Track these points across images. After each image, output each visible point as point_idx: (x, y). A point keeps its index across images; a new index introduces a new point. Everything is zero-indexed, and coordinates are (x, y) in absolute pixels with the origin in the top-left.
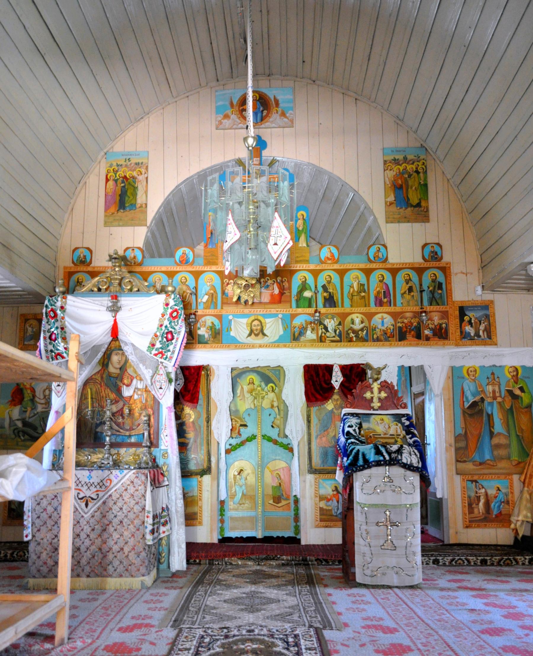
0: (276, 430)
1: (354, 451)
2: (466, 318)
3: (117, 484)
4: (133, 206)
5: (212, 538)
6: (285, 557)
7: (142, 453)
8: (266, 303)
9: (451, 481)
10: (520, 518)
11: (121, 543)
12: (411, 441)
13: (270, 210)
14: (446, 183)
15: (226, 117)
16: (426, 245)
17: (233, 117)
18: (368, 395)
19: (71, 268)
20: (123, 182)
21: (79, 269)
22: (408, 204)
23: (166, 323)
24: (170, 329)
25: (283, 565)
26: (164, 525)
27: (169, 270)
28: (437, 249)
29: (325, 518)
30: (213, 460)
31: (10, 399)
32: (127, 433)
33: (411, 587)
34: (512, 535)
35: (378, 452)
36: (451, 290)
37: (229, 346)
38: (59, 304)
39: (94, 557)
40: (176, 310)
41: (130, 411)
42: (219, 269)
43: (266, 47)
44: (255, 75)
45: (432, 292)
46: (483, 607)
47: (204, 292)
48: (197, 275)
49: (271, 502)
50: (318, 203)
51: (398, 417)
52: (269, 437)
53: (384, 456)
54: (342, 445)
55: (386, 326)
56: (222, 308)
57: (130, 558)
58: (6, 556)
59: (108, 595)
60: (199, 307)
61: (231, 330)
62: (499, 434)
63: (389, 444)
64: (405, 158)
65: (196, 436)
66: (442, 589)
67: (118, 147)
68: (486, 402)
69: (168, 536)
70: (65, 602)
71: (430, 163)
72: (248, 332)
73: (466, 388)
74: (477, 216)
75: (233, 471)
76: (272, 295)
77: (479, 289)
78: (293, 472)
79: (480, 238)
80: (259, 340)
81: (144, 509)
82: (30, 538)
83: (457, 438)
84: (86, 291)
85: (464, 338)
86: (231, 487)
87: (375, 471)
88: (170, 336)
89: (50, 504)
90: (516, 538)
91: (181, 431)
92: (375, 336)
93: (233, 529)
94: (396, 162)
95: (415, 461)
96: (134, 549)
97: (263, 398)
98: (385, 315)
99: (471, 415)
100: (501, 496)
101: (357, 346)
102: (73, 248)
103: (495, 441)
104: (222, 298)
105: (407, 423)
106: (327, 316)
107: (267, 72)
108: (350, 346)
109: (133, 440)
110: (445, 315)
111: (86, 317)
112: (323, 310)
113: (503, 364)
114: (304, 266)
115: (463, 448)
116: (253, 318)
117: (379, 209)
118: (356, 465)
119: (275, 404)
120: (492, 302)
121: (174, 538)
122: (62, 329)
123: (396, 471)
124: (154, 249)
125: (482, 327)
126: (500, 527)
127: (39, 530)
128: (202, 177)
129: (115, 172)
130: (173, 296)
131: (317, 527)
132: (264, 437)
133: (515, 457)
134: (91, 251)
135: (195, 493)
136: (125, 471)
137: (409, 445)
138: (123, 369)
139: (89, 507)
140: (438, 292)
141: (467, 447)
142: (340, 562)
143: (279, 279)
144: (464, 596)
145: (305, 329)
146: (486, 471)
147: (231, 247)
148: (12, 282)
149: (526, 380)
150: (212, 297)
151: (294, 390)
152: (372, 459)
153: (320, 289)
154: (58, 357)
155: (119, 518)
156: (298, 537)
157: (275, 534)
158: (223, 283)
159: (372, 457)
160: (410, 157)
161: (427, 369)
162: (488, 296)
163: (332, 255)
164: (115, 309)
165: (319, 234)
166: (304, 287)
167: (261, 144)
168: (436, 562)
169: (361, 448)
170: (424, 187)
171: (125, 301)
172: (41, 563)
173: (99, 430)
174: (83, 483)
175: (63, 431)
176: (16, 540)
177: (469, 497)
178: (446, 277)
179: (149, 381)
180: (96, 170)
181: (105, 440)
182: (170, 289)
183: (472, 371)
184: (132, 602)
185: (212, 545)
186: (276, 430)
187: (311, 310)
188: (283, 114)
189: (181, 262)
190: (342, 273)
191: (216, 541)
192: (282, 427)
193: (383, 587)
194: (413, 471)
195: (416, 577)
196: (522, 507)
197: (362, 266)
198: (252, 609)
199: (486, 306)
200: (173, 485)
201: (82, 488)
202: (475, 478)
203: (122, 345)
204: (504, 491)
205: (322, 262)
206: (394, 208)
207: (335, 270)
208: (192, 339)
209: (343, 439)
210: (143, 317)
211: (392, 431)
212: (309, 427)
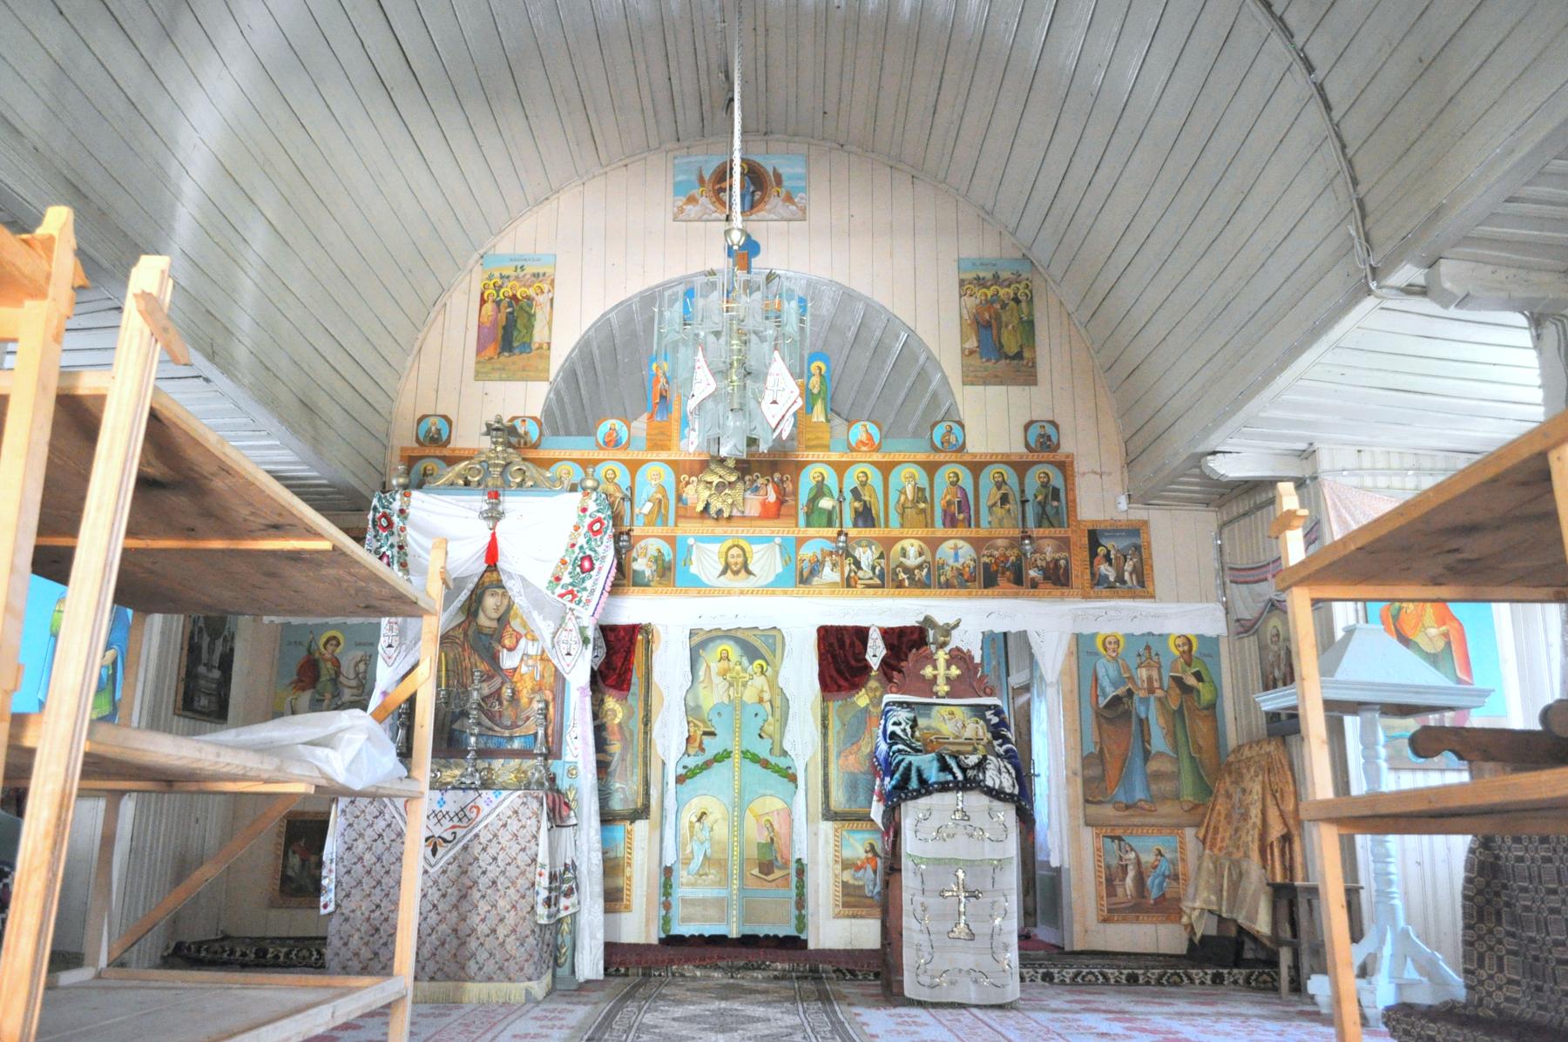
0: (767, 743)
1: (903, 764)
4: (526, 347)
6: (779, 966)
7: (531, 767)
8: (752, 518)
9: (1075, 837)
11: (492, 920)
12: (1001, 750)
13: (766, 347)
14: (1065, 321)
15: (692, 200)
16: (1031, 423)
17: (703, 200)
18: (928, 671)
20: (510, 305)
21: (427, 452)
22: (1000, 352)
23: (582, 541)
25: (776, 978)
26: (568, 894)
28: (1050, 430)
29: (852, 901)
31: (295, 677)
32: (507, 733)
33: (1000, 1007)
34: (1185, 936)
35: (945, 767)
38: (396, 505)
39: (443, 944)
40: (599, 520)
41: (514, 691)
43: (762, 88)
44: (744, 132)
45: (1043, 505)
47: (645, 496)
48: (634, 466)
49: (756, 871)
50: (846, 352)
51: (979, 711)
52: (754, 755)
53: (954, 774)
54: (882, 758)
55: (961, 561)
57: (508, 947)
58: (277, 957)
59: (468, 1009)
62: (1160, 754)
63: (963, 753)
64: (996, 277)
65: (625, 749)
66: (1055, 1011)
68: (1135, 698)
69: (574, 916)
71: (1037, 282)
72: (721, 568)
73: (1101, 672)
75: (689, 815)
76: (764, 504)
77: (1123, 501)
78: (796, 817)
79: (1124, 413)
80: (742, 582)
81: (534, 860)
82: (331, 908)
83: (1087, 761)
85: (1098, 584)
87: (937, 799)
88: (587, 564)
89: (370, 849)
91: (600, 730)
93: (685, 920)
94: (980, 282)
95: (1007, 783)
96: (514, 931)
97: (745, 685)
98: (961, 543)
99: (1110, 721)
100: (1164, 867)
101: (910, 596)
102: (418, 415)
104: (677, 508)
105: (995, 720)
106: (858, 542)
107: (763, 130)
109: (516, 745)
110: (1064, 544)
112: (853, 532)
113: (1166, 631)
115: (1097, 779)
116: (729, 543)
119: (767, 696)
120: (1145, 523)
122: (401, 547)
123: (976, 801)
124: (560, 423)
125: (1128, 566)
126: (1162, 922)
127: (348, 895)
128: (650, 298)
129: (498, 288)
131: (837, 916)
132: (745, 753)
133: (1188, 795)
134: (450, 422)
135: (621, 852)
136: (505, 793)
137: (998, 756)
138: (503, 621)
139: (439, 855)
140: (1053, 505)
141: (1102, 778)
142: (877, 975)
143: (777, 476)
145: (822, 564)
146: (1136, 820)
147: (700, 406)
149: (1207, 660)
151: (801, 670)
152: (932, 780)
153: (848, 495)
155: (490, 875)
157: (762, 931)
158: (678, 482)
159: (933, 775)
160: (1004, 275)
161: (1034, 640)
162: (1139, 514)
165: (848, 406)
166: (820, 490)
167: (746, 252)
168: (1048, 977)
169: (916, 760)
170: (1029, 326)
171: (510, 502)
173: (456, 726)
175: (412, 701)
176: (292, 934)
177: (1108, 867)
180: (465, 285)
181: (467, 744)
182: (590, 483)
183: (1111, 643)
184: (511, 1018)
185: (648, 947)
186: (767, 743)
188: (789, 199)
189: (606, 443)
190: (886, 468)
191: (654, 941)
192: (777, 737)
193: (952, 1005)
194: (1004, 800)
195: (1009, 989)
196: (1202, 883)
197: (921, 457)
199: (1135, 531)
200: (585, 825)
202: (1119, 832)
203: (504, 578)
204: (1168, 856)
205: (851, 449)
206: (976, 361)
207: (873, 463)
208: (623, 578)
209: (883, 747)
210: (540, 533)
211: (969, 733)
212: (825, 735)
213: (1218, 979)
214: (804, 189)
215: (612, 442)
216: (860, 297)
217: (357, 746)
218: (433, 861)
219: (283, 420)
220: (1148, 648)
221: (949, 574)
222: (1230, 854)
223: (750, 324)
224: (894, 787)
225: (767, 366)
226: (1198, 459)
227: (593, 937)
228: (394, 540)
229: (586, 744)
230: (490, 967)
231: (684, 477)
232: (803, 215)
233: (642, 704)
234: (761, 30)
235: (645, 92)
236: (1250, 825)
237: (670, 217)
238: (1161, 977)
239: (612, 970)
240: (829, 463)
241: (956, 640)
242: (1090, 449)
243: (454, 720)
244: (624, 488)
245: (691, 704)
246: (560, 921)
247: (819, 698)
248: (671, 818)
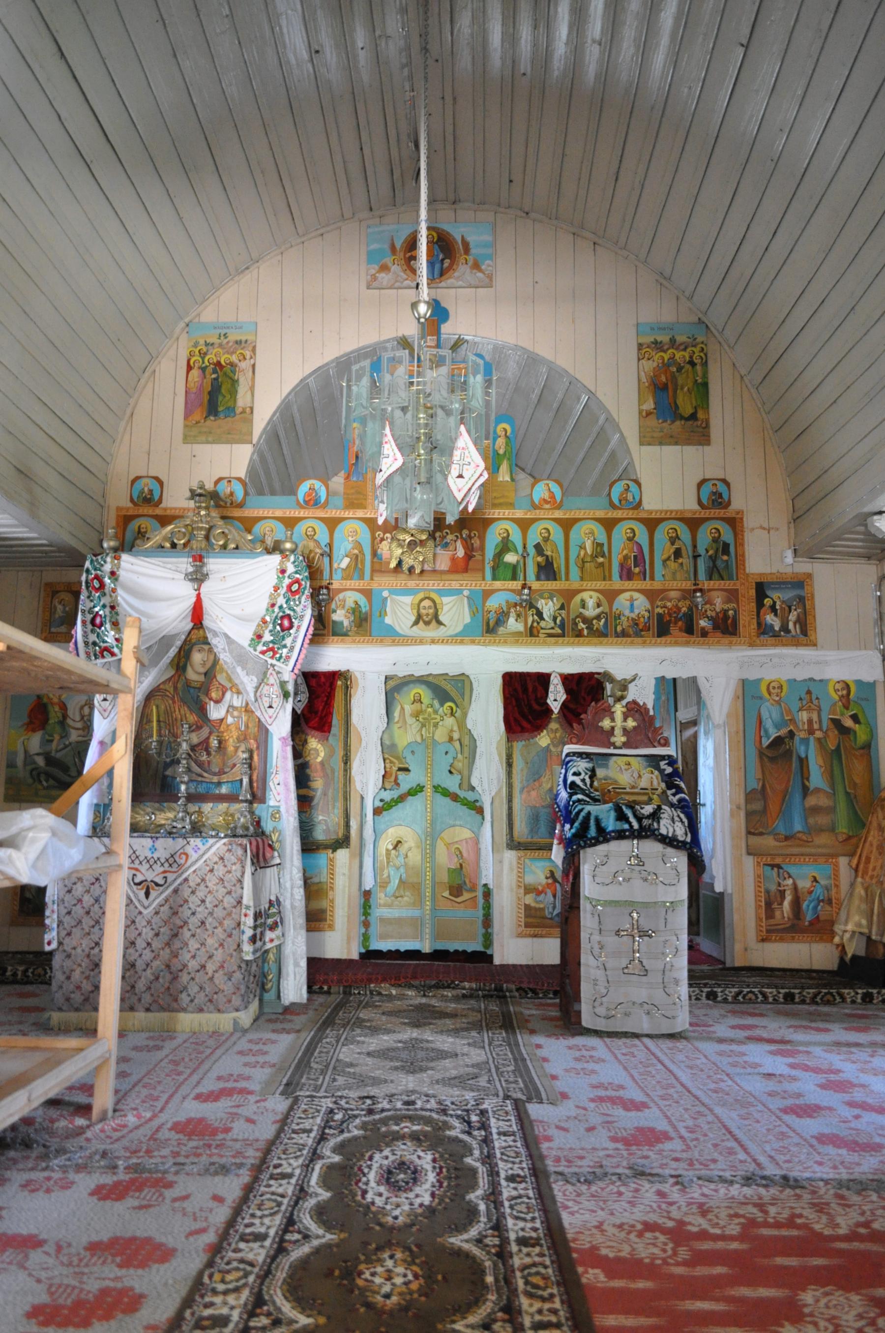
0: (457, 778)
1: (583, 814)
2: (767, 602)
3: (197, 861)
4: (231, 410)
5: (349, 951)
6: (467, 985)
8: (442, 572)
9: (738, 864)
11: (202, 957)
12: (675, 799)
13: (452, 421)
15: (384, 268)
17: (395, 268)
18: (606, 723)
19: (128, 509)
20: (215, 372)
22: (676, 415)
23: (281, 601)
24: (288, 612)
25: (464, 996)
26: (273, 928)
27: (287, 515)
28: (721, 488)
29: (533, 922)
31: (26, 720)
32: (215, 779)
33: (671, 1036)
34: (836, 954)
35: (621, 817)
36: (743, 555)
37: (381, 641)
38: (108, 568)
39: (157, 978)
40: (297, 581)
41: (220, 742)
42: (368, 516)
43: (450, 156)
44: (431, 201)
45: (713, 559)
46: (786, 1071)
47: (342, 552)
48: (332, 524)
49: (446, 894)
51: (653, 761)
53: (630, 824)
54: (562, 804)
55: (636, 611)
56: (372, 579)
57: (217, 981)
58: (15, 974)
59: (179, 1040)
60: (334, 576)
61: (386, 614)
62: (818, 790)
63: (638, 803)
64: (673, 341)
65: (327, 785)
66: (721, 1041)
67: (208, 315)
69: (279, 947)
70: (109, 1051)
71: (713, 349)
72: (413, 618)
73: (765, 715)
74: (788, 436)
75: (386, 844)
76: (453, 559)
78: (482, 846)
81: (239, 902)
82: (54, 945)
83: (750, 796)
84: (152, 547)
85: (764, 633)
86: (382, 870)
87: (615, 846)
88: (286, 623)
89: (88, 891)
92: (619, 629)
93: (383, 937)
94: (657, 346)
95: (681, 831)
96: (222, 967)
97: (436, 725)
98: (636, 595)
99: (772, 759)
100: (819, 892)
101: (588, 644)
102: (132, 477)
103: (811, 801)
104: (372, 563)
105: (669, 770)
106: (541, 594)
107: (451, 197)
108: (579, 644)
109: (224, 790)
110: (733, 595)
111: (151, 589)
112: (536, 585)
113: (826, 676)
114: (507, 513)
115: (758, 812)
116: (421, 595)
117: (629, 423)
119: (456, 736)
120: (810, 576)
121: (288, 950)
122: (113, 608)
123: (650, 848)
125: (793, 617)
126: (816, 942)
127: (69, 934)
129: (203, 355)
130: (292, 558)
131: (520, 935)
132: (436, 788)
133: (843, 828)
134: (161, 483)
135: (324, 877)
137: (672, 805)
138: (210, 674)
139: (151, 897)
140: (723, 559)
141: (765, 810)
142: (556, 993)
143: (465, 533)
144: (756, 1053)
145: (506, 615)
146: (796, 850)
149: (863, 703)
150: (357, 559)
151: (487, 714)
153: (532, 551)
154: (105, 653)
155: (199, 916)
156: (489, 952)
157: (452, 946)
158: (373, 538)
159: (611, 824)
161: (702, 684)
162: (804, 567)
163: (552, 496)
164: (198, 577)
166: (505, 546)
167: (439, 313)
168: (712, 996)
169: (594, 809)
170: (703, 389)
171: (215, 564)
173: (169, 772)
174: (141, 858)
175: (110, 773)
177: (767, 892)
178: (736, 535)
181: (179, 790)
182: (288, 545)
183: (774, 688)
184: (219, 1052)
186: (457, 778)
187: (517, 585)
188: (476, 266)
190: (567, 525)
191: (355, 956)
192: (466, 773)
194: (677, 847)
195: (679, 1020)
197: (600, 514)
198: (412, 1068)
199: (800, 583)
200: (288, 865)
201: (139, 867)
202: (778, 860)
203: (209, 636)
204: (823, 882)
205: (535, 507)
206: (653, 422)
208: (323, 629)
209: (564, 795)
210: (244, 591)
211: (644, 783)
212: (509, 774)
213: (868, 998)
214: (490, 257)
215: (312, 501)
217: (39, 846)
218: (146, 903)
220: (809, 692)
221: (625, 624)
223: (436, 399)
224: (574, 835)
227: (297, 965)
228: (105, 600)
229: (288, 790)
231: (379, 534)
235: (338, 158)
237: (363, 286)
238: (816, 995)
239: (316, 987)
240: (512, 520)
241: (632, 694)
242: (759, 506)
243: (167, 766)
246: (267, 952)
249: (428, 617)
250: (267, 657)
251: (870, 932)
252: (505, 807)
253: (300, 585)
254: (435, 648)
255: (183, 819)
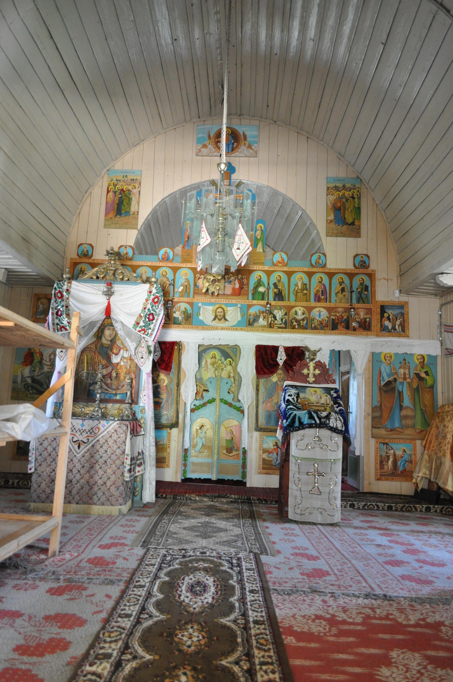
0: (232, 396)
1: (292, 415)
2: (386, 315)
4: (128, 213)
6: (233, 496)
9: (367, 442)
10: (420, 475)
11: (105, 478)
12: (337, 410)
13: (235, 221)
15: (205, 146)
17: (210, 146)
18: (305, 371)
20: (120, 194)
22: (344, 222)
23: (149, 306)
24: (152, 312)
25: (232, 502)
26: (139, 465)
28: (365, 259)
29: (267, 466)
30: (181, 416)
31: (23, 360)
32: (114, 392)
33: (332, 525)
34: (414, 487)
35: (311, 417)
36: (375, 292)
38: (65, 287)
39: (82, 488)
40: (157, 297)
41: (117, 374)
42: (193, 266)
43: (239, 93)
44: (229, 114)
45: (360, 293)
46: (387, 543)
47: (180, 284)
48: (175, 270)
49: (225, 452)
50: (273, 218)
52: (225, 401)
55: (322, 317)
57: (111, 490)
58: (13, 484)
59: (92, 519)
60: (175, 295)
62: (407, 407)
63: (319, 411)
64: (344, 186)
65: (168, 397)
66: (356, 528)
67: (118, 166)
68: (398, 382)
69: (142, 475)
70: (58, 523)
71: (363, 191)
72: (213, 317)
73: (383, 370)
74: (399, 235)
75: (196, 426)
76: (234, 289)
77: (397, 292)
81: (124, 452)
82: (33, 470)
83: (374, 409)
84: (87, 278)
85: (383, 330)
86: (194, 439)
88: (151, 317)
89: (50, 445)
90: (416, 490)
91: (156, 392)
92: (313, 325)
94: (337, 188)
95: (339, 425)
96: (114, 483)
97: (222, 370)
98: (322, 309)
99: (386, 392)
100: (406, 457)
101: (298, 332)
102: (78, 244)
103: (404, 413)
104: (194, 289)
105: (335, 395)
107: (239, 112)
108: (293, 332)
109: (118, 397)
110: (369, 311)
111: (86, 298)
112: (273, 303)
113: (413, 352)
114: (260, 267)
115: (378, 417)
116: (217, 306)
118: (294, 426)
119: (232, 375)
120: (407, 303)
121: (147, 476)
122: (67, 307)
123: (325, 433)
125: (398, 323)
126: (404, 481)
127: (40, 465)
129: (115, 185)
130: (155, 286)
131: (260, 473)
132: (221, 400)
133: (419, 427)
135: (165, 442)
136: (111, 422)
137: (336, 412)
138: (113, 341)
139: (81, 448)
140: (365, 293)
141: (381, 416)
142: (276, 502)
143: (240, 276)
144: (373, 534)
146: (395, 436)
148: (29, 268)
149: (431, 366)
150: (186, 287)
151: (247, 365)
153: (272, 286)
155: (104, 458)
156: (244, 481)
157: (226, 477)
158: (195, 277)
159: (306, 420)
161: (352, 353)
162: (404, 298)
163: (283, 260)
164: (109, 294)
165: (273, 243)
166: (259, 283)
167: (231, 169)
168: (352, 506)
169: (298, 413)
171: (117, 287)
172: (41, 491)
173: (91, 388)
174: (77, 429)
175: (63, 387)
177: (381, 456)
178: (371, 282)
179: (133, 352)
180: (100, 184)
181: (96, 397)
183: (388, 357)
185: (177, 483)
186: (232, 396)
188: (250, 147)
189: (162, 258)
190: (289, 274)
191: (179, 481)
192: (236, 393)
193: (309, 523)
194: (338, 433)
195: (336, 517)
196: (423, 466)
197: (306, 269)
198: (205, 536)
199: (402, 306)
200: (148, 435)
201: (76, 434)
202: (387, 441)
203: (113, 322)
204: (408, 452)
205: (274, 265)
206: (333, 225)
208: (169, 321)
209: (283, 405)
210: (131, 301)
211: (323, 401)
212: (257, 394)
213: (428, 510)
215: (166, 259)
216: (280, 194)
217: (27, 422)
219: (13, 246)
220: (404, 360)
221: (316, 323)
222: (437, 454)
223: (228, 211)
224: (288, 425)
225: (236, 231)
226: (434, 276)
227: (150, 484)
230: (103, 499)
232: (256, 155)
233: (176, 377)
234: (239, 64)
236: (447, 441)
238: (403, 507)
239: (159, 495)
241: (319, 357)
242: (383, 268)
244: (170, 279)
245: (198, 377)
246: (136, 477)
247: (255, 377)
248: (188, 428)
249: (221, 317)
250: (141, 334)
251: (430, 477)
252: (255, 410)
253: (158, 299)
254: (222, 331)
255: (98, 411)
